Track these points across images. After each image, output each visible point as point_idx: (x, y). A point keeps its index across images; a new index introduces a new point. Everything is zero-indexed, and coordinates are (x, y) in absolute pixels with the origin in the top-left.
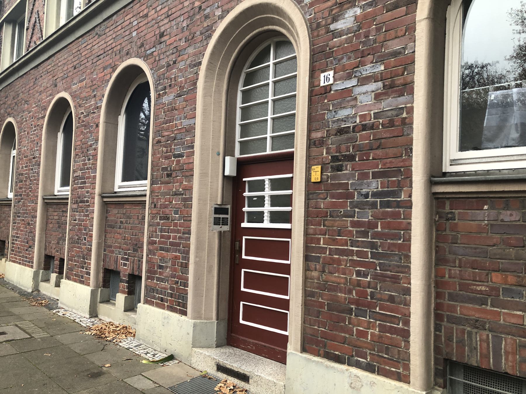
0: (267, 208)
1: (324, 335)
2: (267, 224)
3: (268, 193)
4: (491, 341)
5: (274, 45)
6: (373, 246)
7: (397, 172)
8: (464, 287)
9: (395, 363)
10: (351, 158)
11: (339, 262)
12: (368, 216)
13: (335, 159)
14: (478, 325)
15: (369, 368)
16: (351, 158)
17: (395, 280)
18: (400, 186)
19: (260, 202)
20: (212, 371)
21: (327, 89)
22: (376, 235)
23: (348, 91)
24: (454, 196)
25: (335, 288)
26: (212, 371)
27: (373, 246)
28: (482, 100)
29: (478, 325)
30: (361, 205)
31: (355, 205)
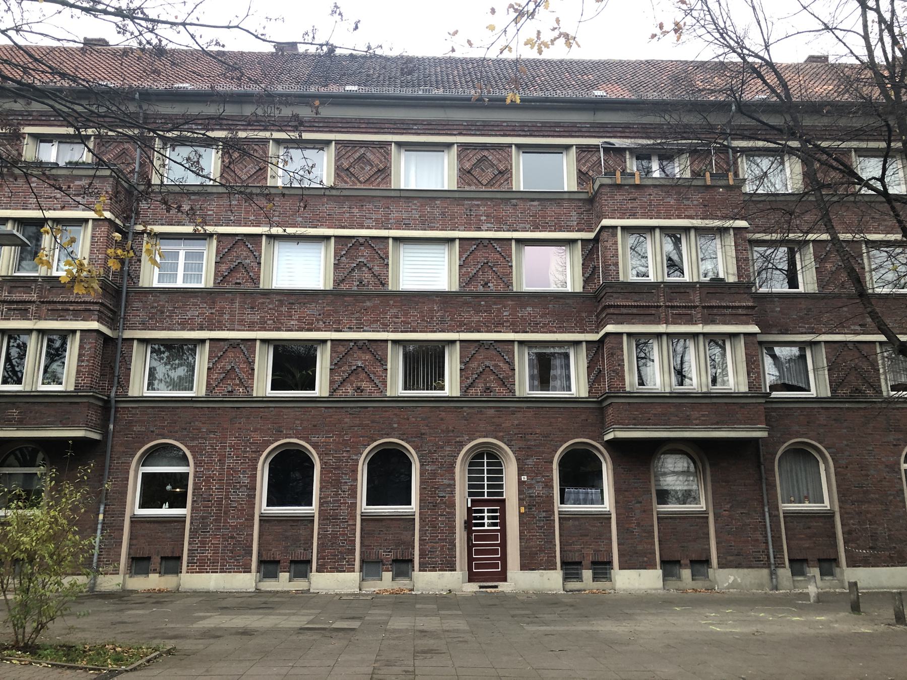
0: (486, 521)
1: (528, 563)
2: (486, 528)
3: (486, 514)
4: (573, 628)
5: (664, 595)
6: (544, 533)
7: (550, 511)
8: (567, 542)
9: (552, 565)
10: (535, 506)
11: (532, 539)
12: (542, 524)
13: (529, 505)
14: (570, 551)
15: (545, 569)
16: (535, 506)
17: (551, 542)
18: (551, 515)
19: (483, 518)
20: (478, 589)
21: (524, 482)
22: (545, 529)
23: (531, 484)
24: (61, 400)
25: (531, 547)
26: (478, 589)
27: (544, 533)
28: (483, 218)
29: (570, 551)
30: (539, 521)
31: (536, 520)
